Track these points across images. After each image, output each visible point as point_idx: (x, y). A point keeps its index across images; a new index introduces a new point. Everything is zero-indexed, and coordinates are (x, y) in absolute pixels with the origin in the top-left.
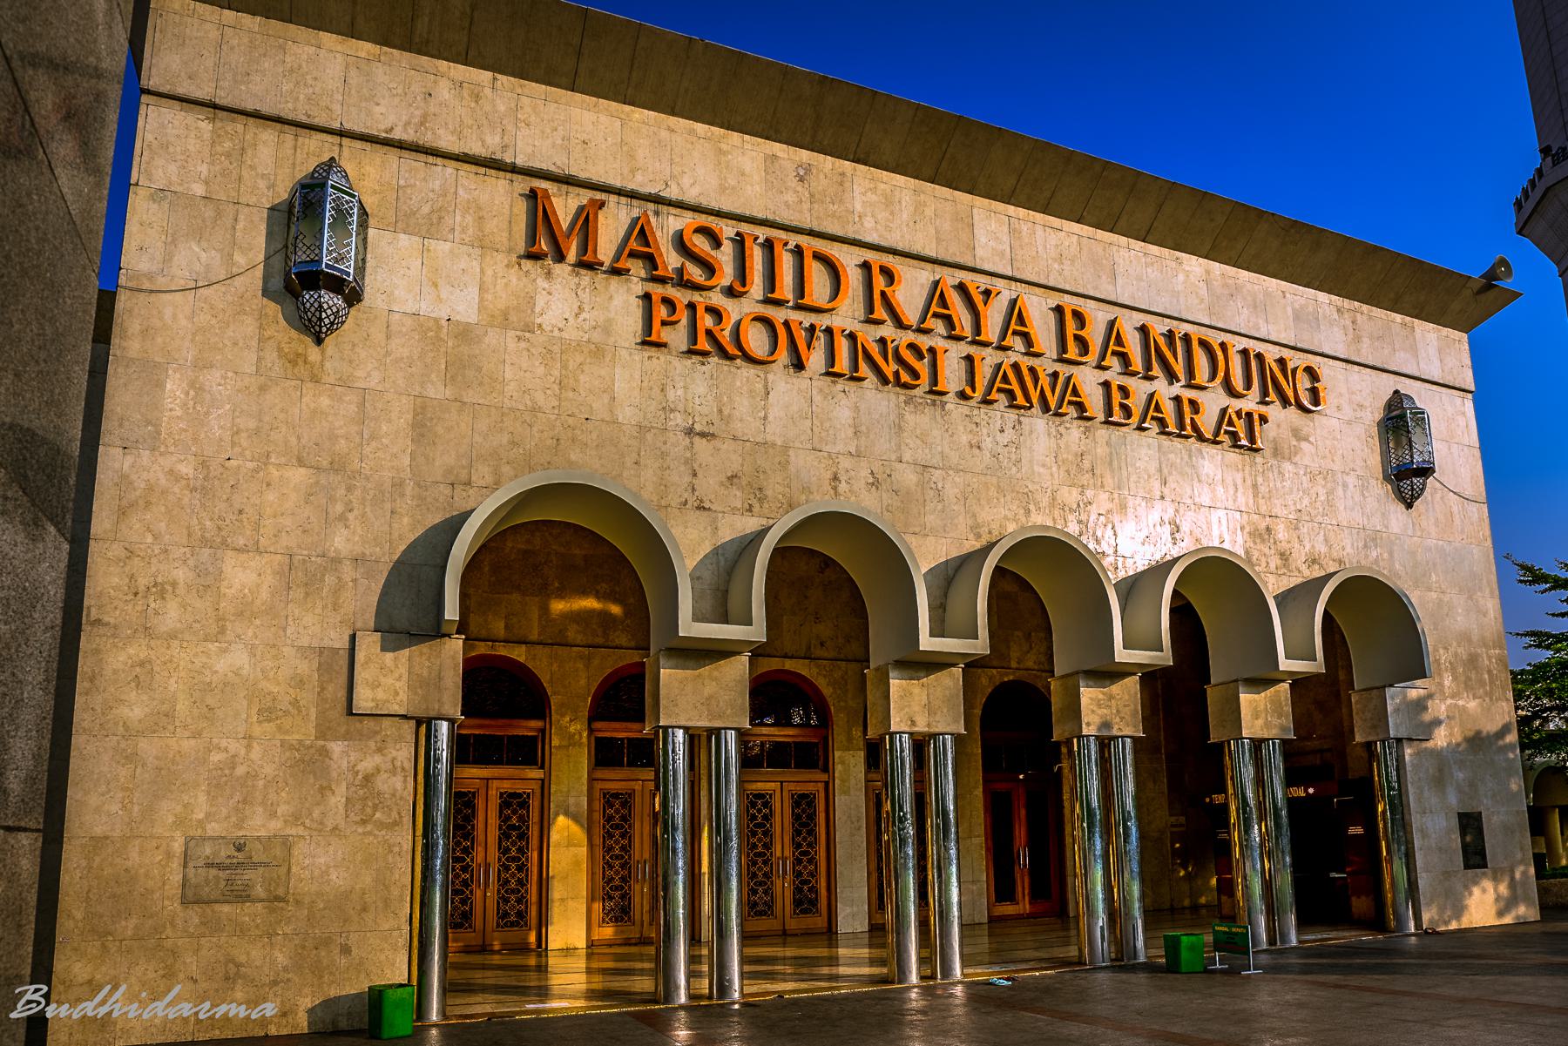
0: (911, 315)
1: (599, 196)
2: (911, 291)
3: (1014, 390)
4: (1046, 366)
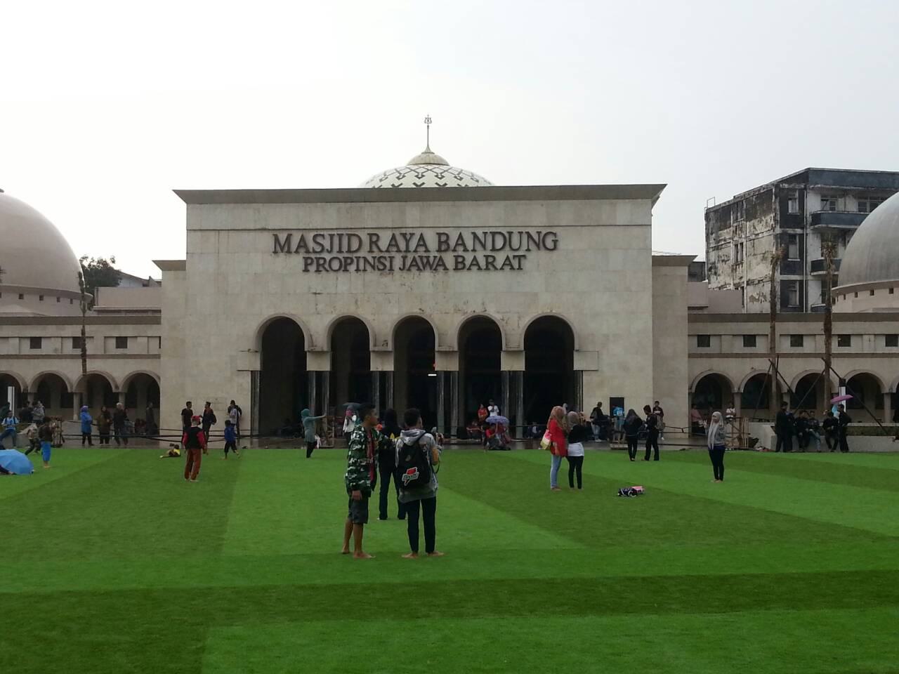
0: (384, 248)
1: (290, 232)
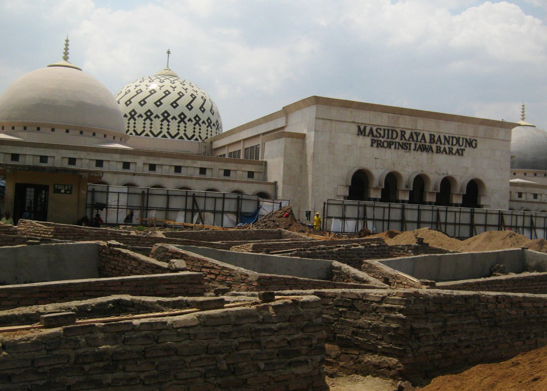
2: (407, 136)
3: (424, 149)
4: (427, 144)
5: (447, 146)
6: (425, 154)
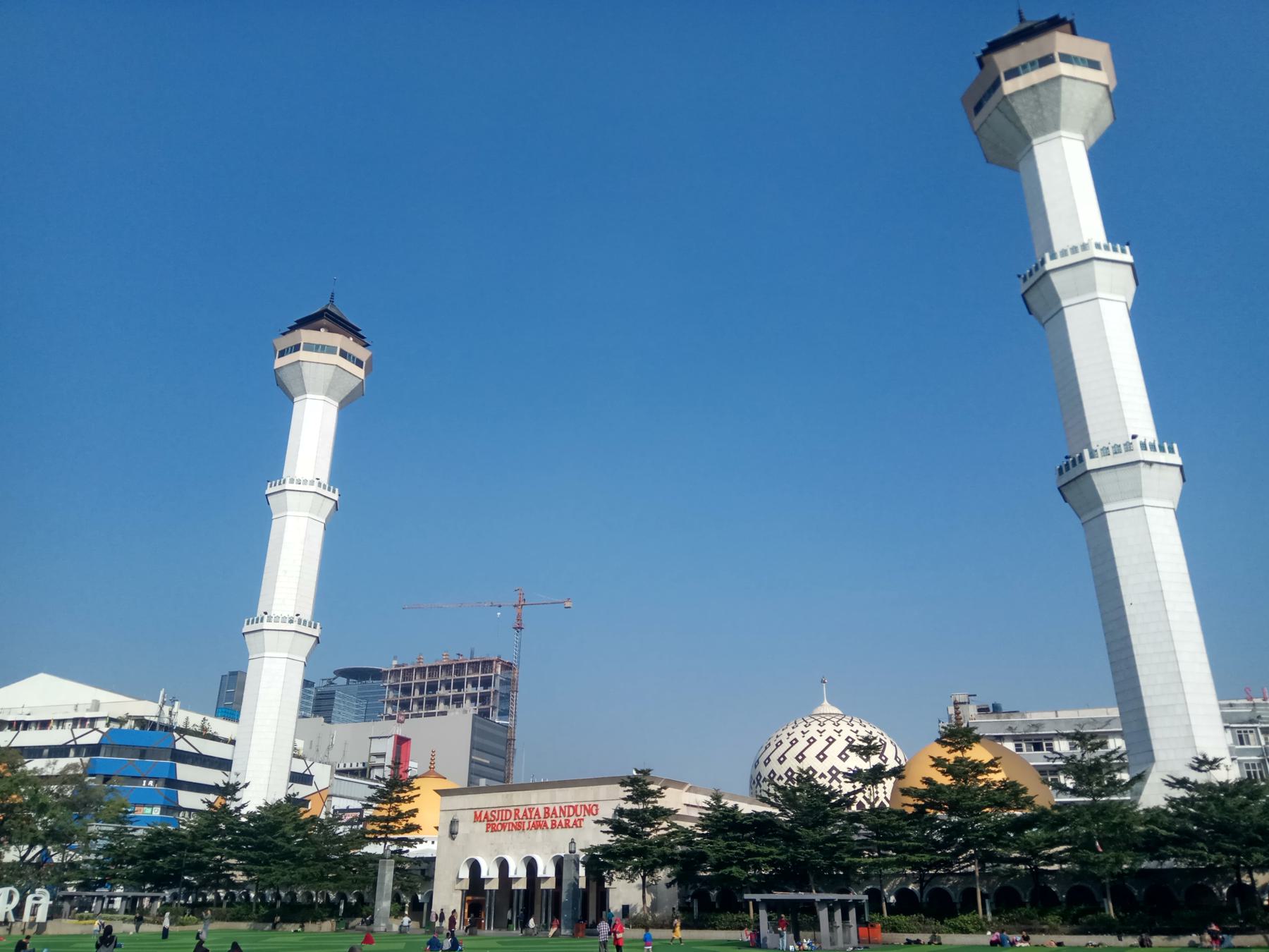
3: (538, 826)
5: (563, 819)
6: (539, 831)
